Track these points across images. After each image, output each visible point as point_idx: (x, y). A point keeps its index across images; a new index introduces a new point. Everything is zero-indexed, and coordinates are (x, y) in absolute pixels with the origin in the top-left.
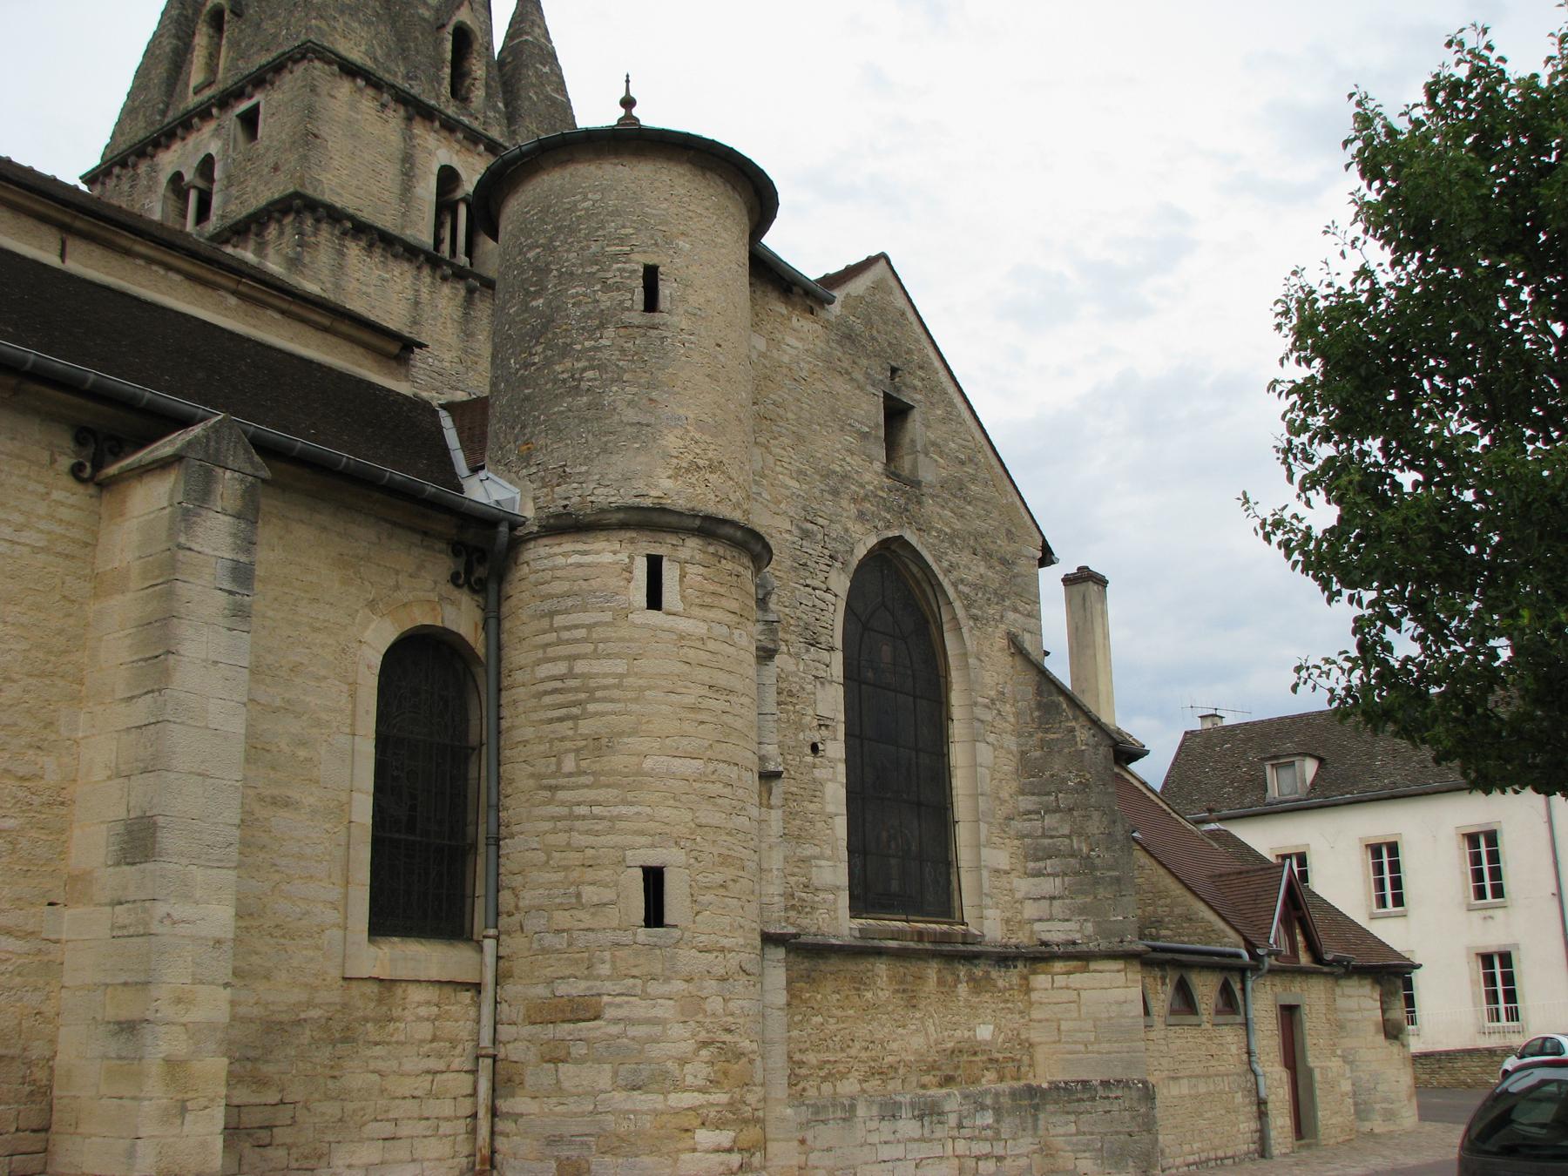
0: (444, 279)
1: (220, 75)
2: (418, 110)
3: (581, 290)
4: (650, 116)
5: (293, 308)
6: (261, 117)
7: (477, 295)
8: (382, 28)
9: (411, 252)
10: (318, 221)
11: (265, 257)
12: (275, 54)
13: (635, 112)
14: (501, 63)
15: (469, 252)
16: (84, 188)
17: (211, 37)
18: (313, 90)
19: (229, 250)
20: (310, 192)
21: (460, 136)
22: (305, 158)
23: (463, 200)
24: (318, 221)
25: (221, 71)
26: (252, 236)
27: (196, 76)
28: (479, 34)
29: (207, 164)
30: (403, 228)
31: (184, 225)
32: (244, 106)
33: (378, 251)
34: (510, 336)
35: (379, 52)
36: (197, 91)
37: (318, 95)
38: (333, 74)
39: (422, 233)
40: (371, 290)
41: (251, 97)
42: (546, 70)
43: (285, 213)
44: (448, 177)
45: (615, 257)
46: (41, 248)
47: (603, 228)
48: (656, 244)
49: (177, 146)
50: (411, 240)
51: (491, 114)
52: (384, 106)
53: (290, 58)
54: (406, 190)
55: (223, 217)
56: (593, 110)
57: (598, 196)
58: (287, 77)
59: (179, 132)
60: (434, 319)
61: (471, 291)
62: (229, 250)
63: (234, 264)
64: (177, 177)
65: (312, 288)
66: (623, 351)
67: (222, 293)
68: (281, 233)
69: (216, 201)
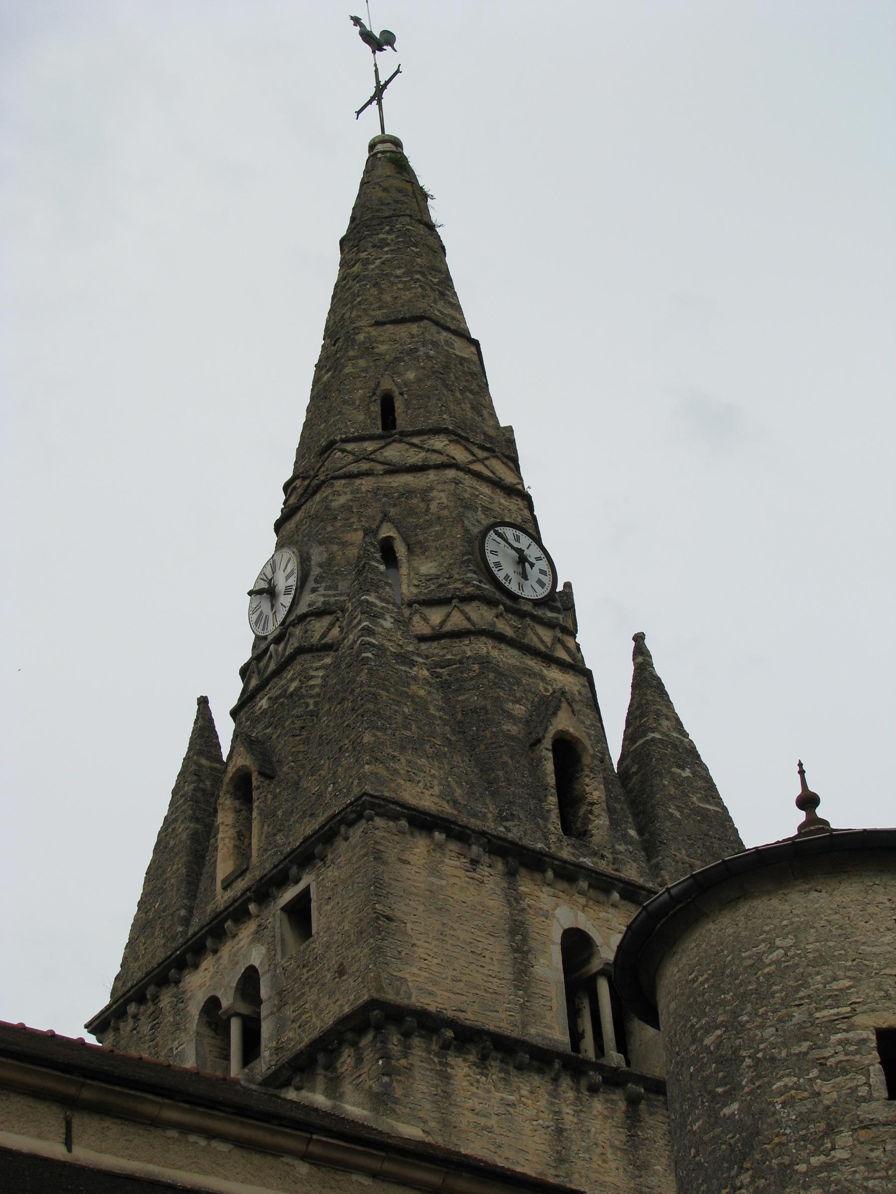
0: (593, 1089)
1: (254, 859)
2: (520, 860)
3: (790, 1081)
4: (842, 814)
5: (388, 1166)
6: (314, 905)
7: (642, 1106)
8: (457, 759)
9: (536, 1059)
10: (407, 1035)
11: (341, 1097)
12: (321, 819)
13: (821, 812)
14: (624, 774)
15: (622, 1045)
16: (91, 1039)
17: (238, 811)
18: (378, 857)
19: (291, 1094)
20: (390, 996)
21: (584, 884)
22: (378, 951)
23: (602, 972)
24: (407, 1035)
25: (254, 853)
26: (320, 1071)
27: (224, 867)
28: (588, 743)
29: (251, 977)
30: (525, 1025)
31: (228, 1069)
32: (289, 894)
33: (494, 1065)
34: (699, 1164)
35: (458, 792)
36: (227, 884)
37: (385, 863)
38: (402, 832)
39: (552, 1029)
40: (493, 1122)
41: (297, 882)
42: (687, 773)
43: (361, 1031)
44: (576, 944)
45: (831, 1026)
46: (39, 1136)
47: (805, 985)
48: (888, 997)
49: (208, 963)
50: (538, 1041)
51: (621, 848)
52: (474, 862)
53: (341, 822)
54: (522, 974)
55: (277, 1050)
56: (763, 820)
57: (789, 941)
58: (341, 846)
59: (209, 943)
60: (588, 1150)
61: (633, 1102)
62: (291, 1094)
63: (300, 1115)
64: (213, 1004)
65: (411, 1131)
66: (869, 1163)
67: (286, 1159)
68: (359, 1060)
69: (266, 1029)
